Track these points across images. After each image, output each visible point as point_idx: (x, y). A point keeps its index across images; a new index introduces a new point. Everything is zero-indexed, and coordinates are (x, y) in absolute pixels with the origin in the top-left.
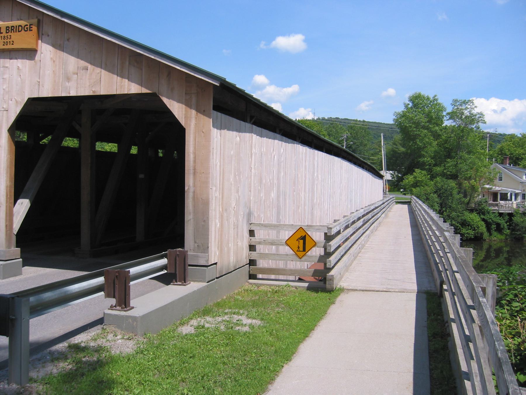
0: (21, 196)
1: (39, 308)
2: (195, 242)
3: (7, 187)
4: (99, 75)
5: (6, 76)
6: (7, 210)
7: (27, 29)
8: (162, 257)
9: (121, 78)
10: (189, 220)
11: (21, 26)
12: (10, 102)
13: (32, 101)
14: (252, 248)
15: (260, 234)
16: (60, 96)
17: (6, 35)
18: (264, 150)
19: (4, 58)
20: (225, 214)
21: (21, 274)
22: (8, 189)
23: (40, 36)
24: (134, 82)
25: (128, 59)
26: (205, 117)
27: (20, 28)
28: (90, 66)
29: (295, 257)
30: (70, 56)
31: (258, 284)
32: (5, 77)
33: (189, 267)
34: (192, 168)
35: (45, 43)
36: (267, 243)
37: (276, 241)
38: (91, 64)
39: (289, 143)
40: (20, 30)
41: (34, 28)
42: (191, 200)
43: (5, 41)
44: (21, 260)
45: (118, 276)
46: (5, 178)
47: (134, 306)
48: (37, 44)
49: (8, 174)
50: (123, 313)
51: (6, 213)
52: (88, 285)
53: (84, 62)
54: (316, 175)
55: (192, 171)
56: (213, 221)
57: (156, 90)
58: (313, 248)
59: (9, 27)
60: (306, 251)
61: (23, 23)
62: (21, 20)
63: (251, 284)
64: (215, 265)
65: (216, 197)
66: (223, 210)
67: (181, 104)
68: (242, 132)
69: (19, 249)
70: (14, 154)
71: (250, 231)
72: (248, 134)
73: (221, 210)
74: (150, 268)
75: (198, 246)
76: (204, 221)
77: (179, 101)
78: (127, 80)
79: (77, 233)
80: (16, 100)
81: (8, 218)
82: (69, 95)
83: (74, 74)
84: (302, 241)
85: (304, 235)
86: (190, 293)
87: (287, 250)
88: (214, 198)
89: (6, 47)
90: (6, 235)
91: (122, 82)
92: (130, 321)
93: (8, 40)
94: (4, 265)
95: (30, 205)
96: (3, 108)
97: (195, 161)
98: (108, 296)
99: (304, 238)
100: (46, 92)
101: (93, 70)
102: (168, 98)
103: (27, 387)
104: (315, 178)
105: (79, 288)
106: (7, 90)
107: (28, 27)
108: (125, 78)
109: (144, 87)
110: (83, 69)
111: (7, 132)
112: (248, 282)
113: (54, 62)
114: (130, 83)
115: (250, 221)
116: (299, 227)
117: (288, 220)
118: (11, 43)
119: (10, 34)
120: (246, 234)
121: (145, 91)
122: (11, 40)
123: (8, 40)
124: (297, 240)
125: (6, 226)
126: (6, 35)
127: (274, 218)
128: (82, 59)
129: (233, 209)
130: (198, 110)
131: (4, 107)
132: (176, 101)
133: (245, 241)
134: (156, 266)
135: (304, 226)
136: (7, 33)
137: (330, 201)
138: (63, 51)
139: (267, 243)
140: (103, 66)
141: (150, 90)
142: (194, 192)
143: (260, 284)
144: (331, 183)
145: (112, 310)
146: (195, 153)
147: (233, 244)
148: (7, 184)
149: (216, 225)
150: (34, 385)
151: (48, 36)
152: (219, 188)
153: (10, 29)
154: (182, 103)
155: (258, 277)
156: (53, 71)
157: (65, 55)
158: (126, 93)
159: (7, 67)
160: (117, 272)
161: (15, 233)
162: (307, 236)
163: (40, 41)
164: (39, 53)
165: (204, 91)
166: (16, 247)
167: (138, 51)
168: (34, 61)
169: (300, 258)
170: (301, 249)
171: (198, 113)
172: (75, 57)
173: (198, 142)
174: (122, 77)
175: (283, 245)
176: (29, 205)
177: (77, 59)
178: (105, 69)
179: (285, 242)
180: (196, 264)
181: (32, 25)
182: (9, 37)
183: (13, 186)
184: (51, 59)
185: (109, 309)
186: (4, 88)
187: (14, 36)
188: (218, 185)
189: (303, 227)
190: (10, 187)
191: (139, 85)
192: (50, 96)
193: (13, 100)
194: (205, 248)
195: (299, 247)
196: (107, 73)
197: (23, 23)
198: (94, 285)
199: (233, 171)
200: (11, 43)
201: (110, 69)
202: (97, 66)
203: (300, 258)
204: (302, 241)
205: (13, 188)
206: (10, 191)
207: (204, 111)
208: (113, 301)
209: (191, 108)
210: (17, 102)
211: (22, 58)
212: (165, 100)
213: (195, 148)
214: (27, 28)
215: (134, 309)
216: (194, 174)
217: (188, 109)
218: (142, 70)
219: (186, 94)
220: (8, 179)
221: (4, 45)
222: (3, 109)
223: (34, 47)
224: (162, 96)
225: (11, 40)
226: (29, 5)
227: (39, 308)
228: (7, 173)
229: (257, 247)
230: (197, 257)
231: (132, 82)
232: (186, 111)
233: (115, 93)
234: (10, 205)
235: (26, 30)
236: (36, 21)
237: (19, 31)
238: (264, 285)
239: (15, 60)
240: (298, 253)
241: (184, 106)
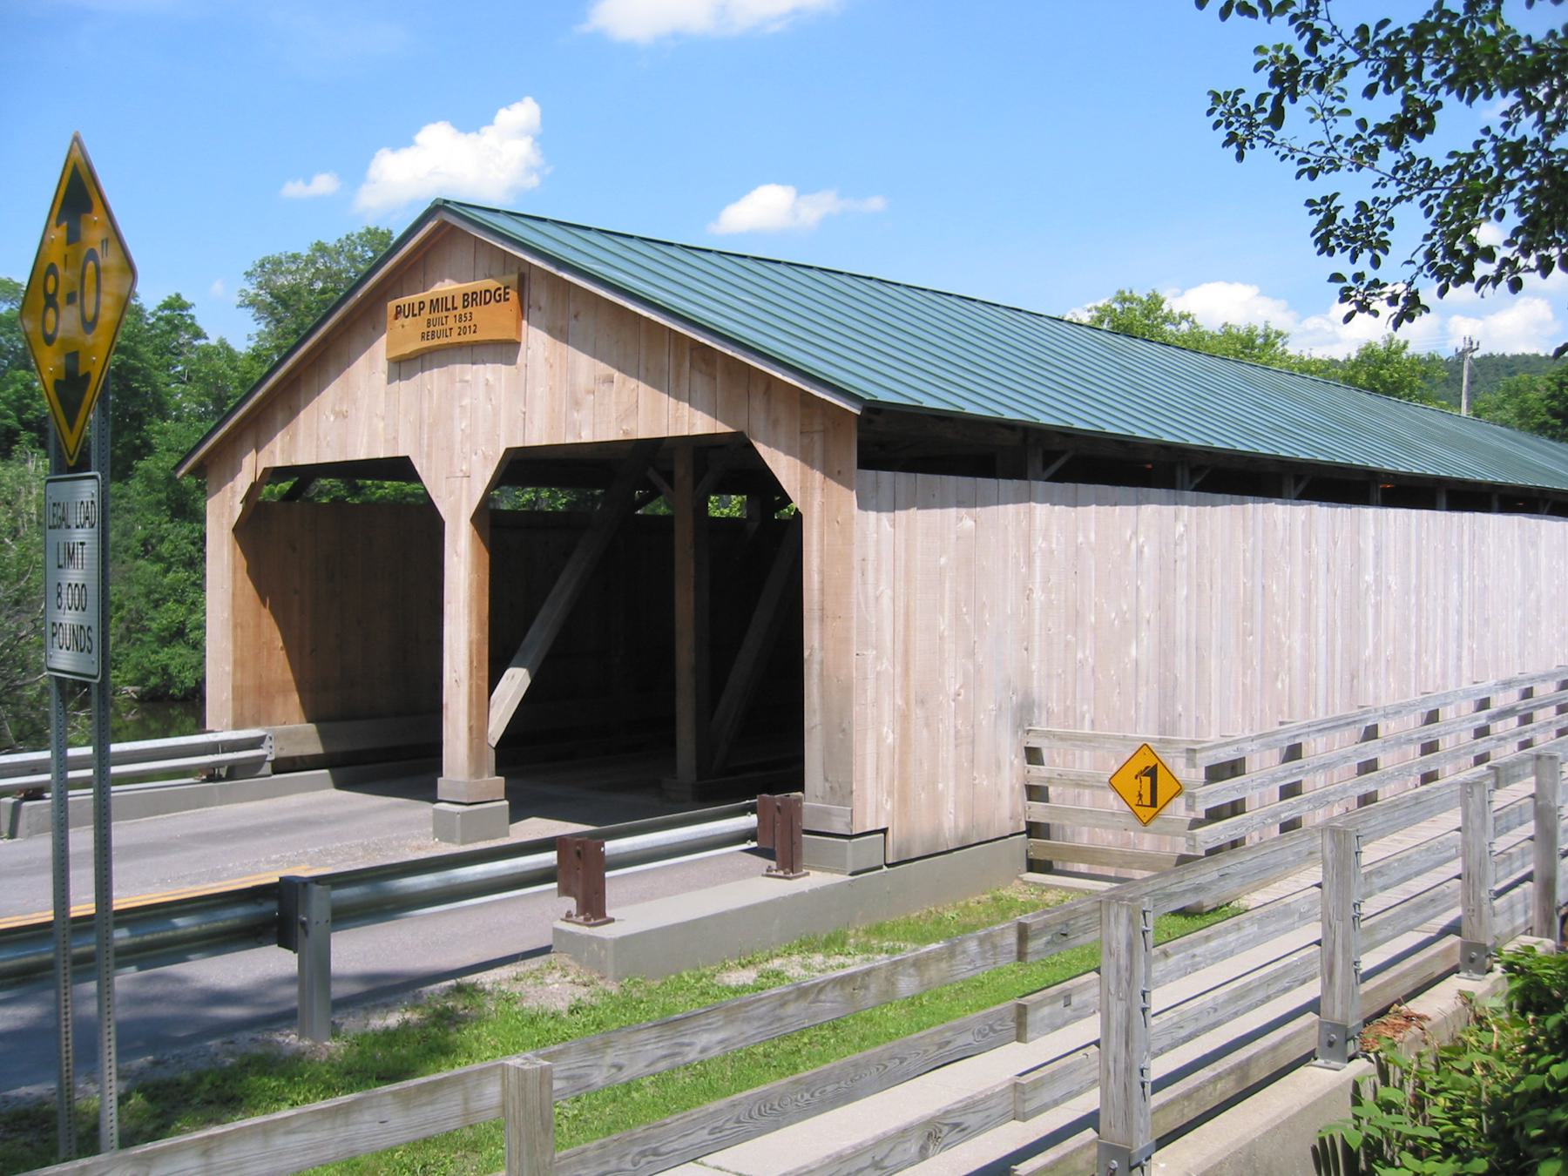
0: (514, 661)
1: (388, 907)
2: (826, 780)
3: (471, 643)
4: (635, 394)
5: (466, 401)
6: (471, 693)
7: (499, 296)
8: (742, 812)
9: (675, 401)
10: (813, 728)
11: (488, 291)
12: (474, 457)
14: (1036, 793)
15: (1056, 762)
16: (562, 442)
18: (1086, 537)
19: (462, 363)
20: (918, 713)
21: (507, 835)
22: (474, 647)
23: (524, 310)
24: (702, 410)
25: (688, 358)
26: (841, 487)
28: (617, 375)
29: (1133, 821)
30: (581, 354)
31: (1042, 884)
32: (463, 403)
33: (803, 836)
34: (816, 607)
35: (533, 326)
36: (1068, 782)
37: (1087, 779)
38: (619, 370)
39: (1213, 506)
40: (487, 300)
41: (513, 295)
42: (816, 681)
43: (462, 324)
44: (506, 803)
45: (582, 853)
46: (467, 625)
47: (616, 918)
48: (519, 329)
49: (474, 614)
50: (585, 930)
51: (470, 700)
52: (510, 868)
53: (606, 366)
54: (1369, 577)
55: (816, 614)
56: (869, 732)
57: (742, 427)
58: (1175, 799)
59: (467, 294)
60: (1159, 806)
61: (491, 284)
62: (491, 277)
63: (1026, 883)
64: (882, 835)
65: (878, 673)
66: (907, 704)
67: (792, 458)
68: (984, 505)
69: (502, 778)
70: (487, 571)
71: (1026, 749)
72: (1011, 508)
73: (899, 702)
74: (699, 836)
75: (831, 788)
76: (844, 730)
77: (789, 452)
78: (687, 405)
79: (671, 742)
80: (484, 454)
81: (475, 712)
83: (588, 392)
84: (1149, 778)
85: (1152, 765)
86: (784, 898)
87: (1112, 802)
88: (871, 676)
89: (463, 338)
90: (471, 748)
91: (678, 409)
92: (595, 946)
93: (467, 324)
94: (463, 814)
95: (529, 681)
96: (462, 471)
97: (822, 590)
98: (565, 891)
99: (1152, 773)
101: (624, 383)
102: (768, 444)
104: (1363, 587)
105: (485, 873)
106: (468, 431)
107: (502, 292)
108: (683, 401)
109: (721, 421)
110: (604, 382)
111: (469, 522)
112: (1021, 879)
113: (551, 366)
114: (692, 409)
115: (1030, 725)
116: (1141, 744)
117: (1413, 697)
118: (473, 328)
119: (469, 309)
120: (1019, 760)
121: (722, 428)
124: (1136, 778)
125: (470, 728)
127: (1142, 712)
128: (602, 360)
129: (952, 697)
130: (828, 473)
131: (464, 468)
132: (783, 451)
133: (1011, 773)
134: (718, 832)
135: (1153, 741)
136: (464, 307)
137: (1460, 646)
138: (567, 342)
139: (1068, 782)
140: (642, 372)
141: (731, 427)
142: (822, 663)
143: (1046, 885)
144: (1461, 594)
145: (567, 921)
146: (822, 572)
147: (952, 784)
148: (470, 636)
149: (880, 740)
151: (540, 309)
152: (890, 651)
153: (470, 300)
154: (795, 456)
155: (1055, 867)
156: (550, 389)
157: (570, 351)
158: (686, 433)
159: (467, 382)
160: (578, 843)
161: (494, 744)
162: (1160, 768)
163: (525, 323)
164: (523, 346)
165: (839, 425)
166: (497, 775)
167: (701, 340)
168: (514, 367)
169: (1145, 824)
170: (1147, 800)
171: (827, 479)
172: (590, 355)
173: (828, 545)
174: (678, 398)
175: (1103, 787)
176: (528, 681)
177: (593, 360)
178: (646, 382)
179: (1107, 780)
180: (827, 831)
181: (508, 287)
182: (468, 315)
183: (487, 641)
184: (546, 359)
185: (562, 920)
186: (463, 427)
187: (479, 313)
188: (889, 644)
189: (1149, 744)
190: (479, 643)
191: (710, 414)
192: (544, 443)
193: (479, 452)
194: (843, 793)
195: (1140, 795)
196: (649, 388)
197: (491, 284)
198: (527, 868)
199: (947, 601)
200: (473, 328)
201: (655, 380)
202: (631, 376)
203: (1145, 824)
204: (1147, 780)
205: (487, 646)
206: (479, 653)
207: (839, 472)
208: (571, 904)
209: (812, 466)
211: (494, 362)
212: (762, 449)
213: (822, 558)
214: (500, 295)
215: (616, 923)
216: (822, 619)
217: (807, 468)
218: (715, 379)
219: (801, 433)
220: (474, 626)
221: (459, 334)
222: (462, 474)
223: (512, 336)
224: (756, 440)
225: (471, 324)
226: (500, 246)
227: (388, 907)
228: (470, 612)
229: (1052, 791)
230: (828, 813)
231: (697, 409)
232: (803, 473)
233: (665, 435)
234: (479, 682)
235: (498, 298)
236: (514, 278)
237: (486, 303)
238: (1055, 887)
239: (482, 366)
240: (1139, 810)
241: (798, 462)
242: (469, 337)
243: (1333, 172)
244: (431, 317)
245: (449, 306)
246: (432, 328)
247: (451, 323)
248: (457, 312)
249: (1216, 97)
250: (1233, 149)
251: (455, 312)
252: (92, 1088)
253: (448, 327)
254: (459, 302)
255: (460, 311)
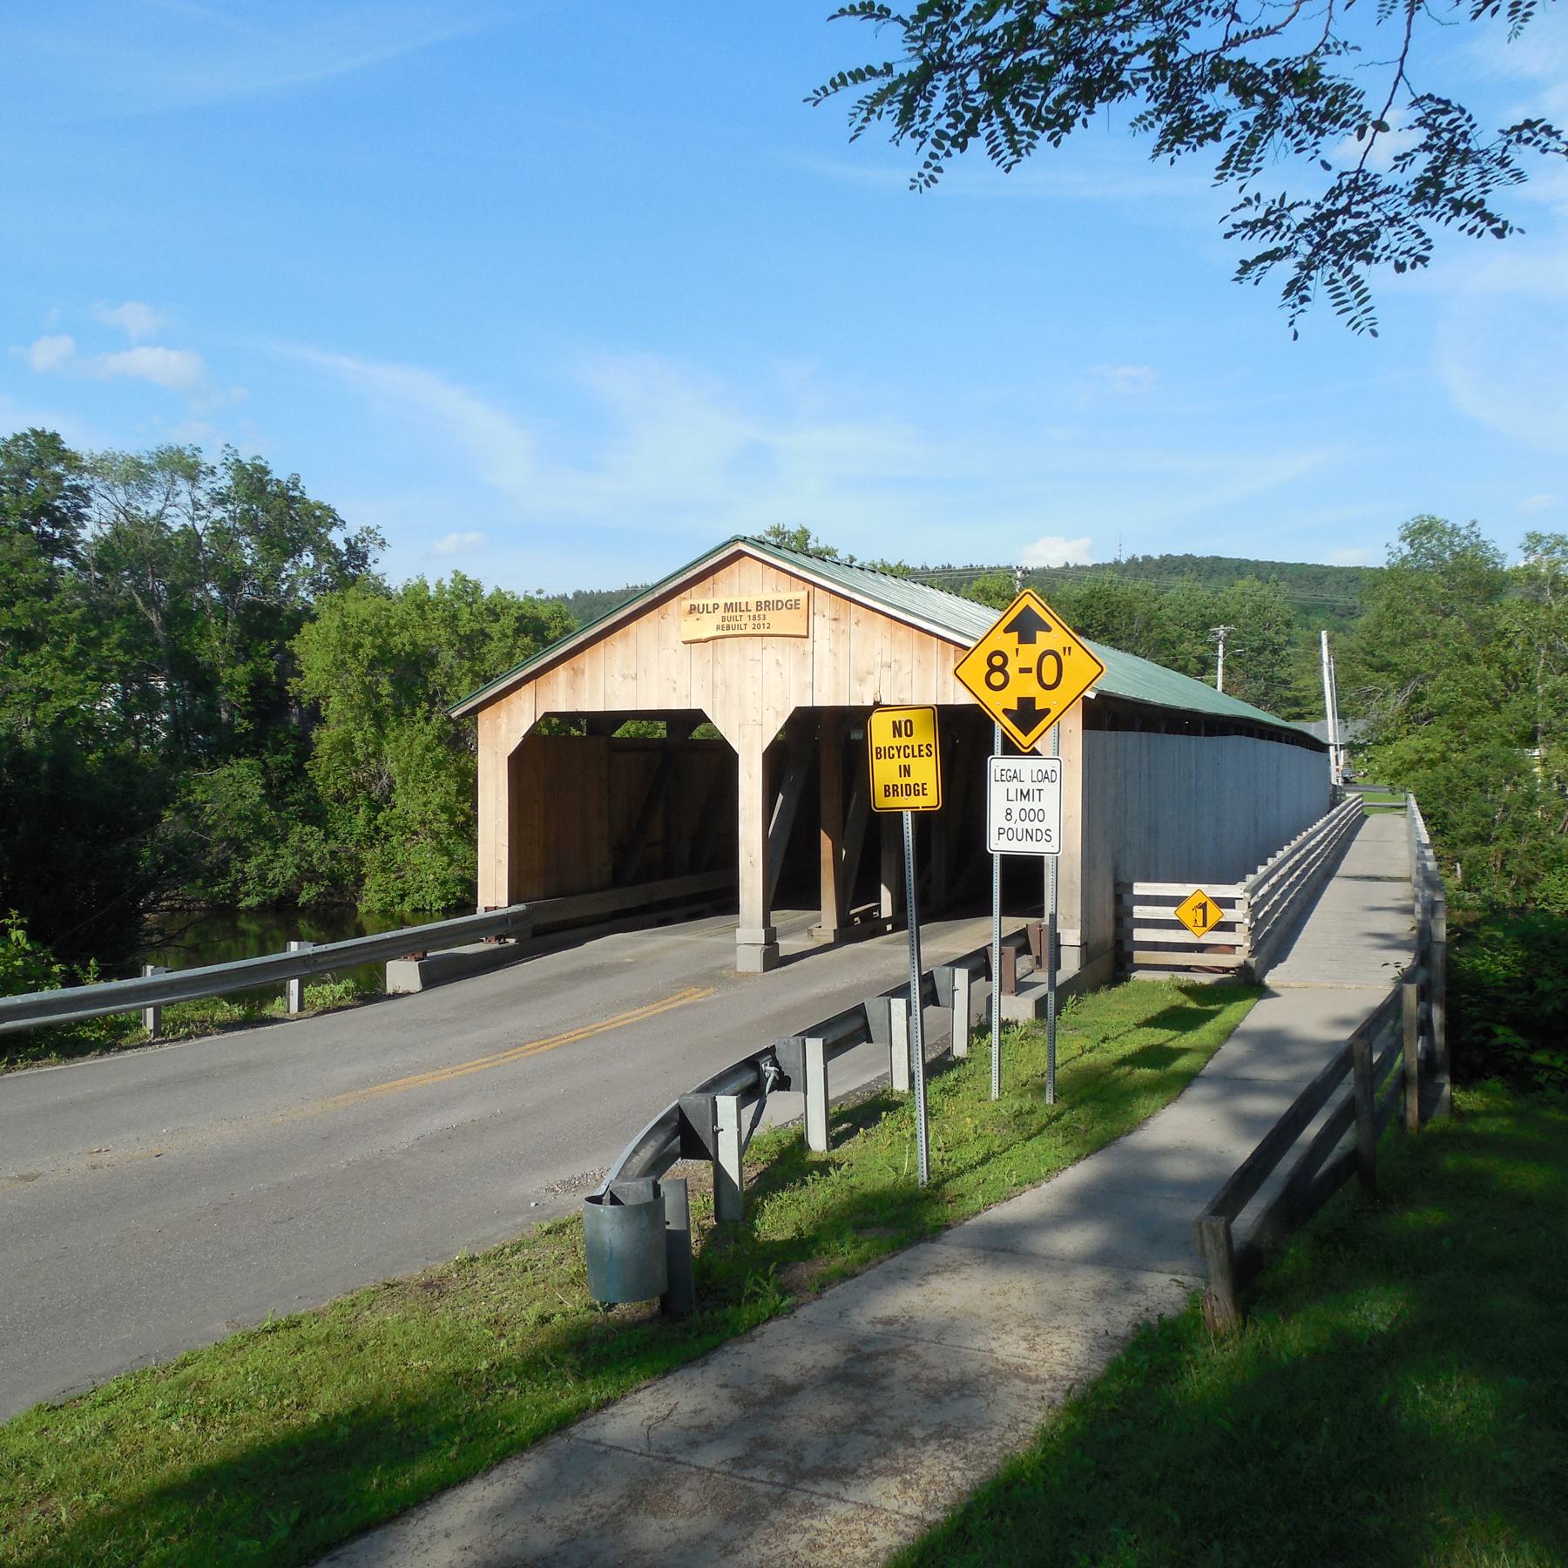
13: (798, 709)
17: (757, 613)
27: (780, 604)
43: (756, 622)
82: (861, 704)
93: (761, 622)
100: (825, 699)
103: (980, 20)
118: (766, 626)
122: (765, 622)
123: (761, 622)
126: (757, 613)
150: (782, 1482)
153: (891, 790)
158: (952, 703)
170: (1200, 923)
182: (762, 617)
187: (771, 616)
200: (766, 626)
210: (777, 713)
242: (762, 631)
243: (1534, 120)
244: (726, 615)
245: (743, 608)
246: (726, 623)
247: (745, 620)
248: (751, 614)
249: (1132, 125)
250: (1529, 18)
251: (749, 613)
252: (847, 1246)
253: (742, 623)
254: (752, 607)
255: (754, 612)
